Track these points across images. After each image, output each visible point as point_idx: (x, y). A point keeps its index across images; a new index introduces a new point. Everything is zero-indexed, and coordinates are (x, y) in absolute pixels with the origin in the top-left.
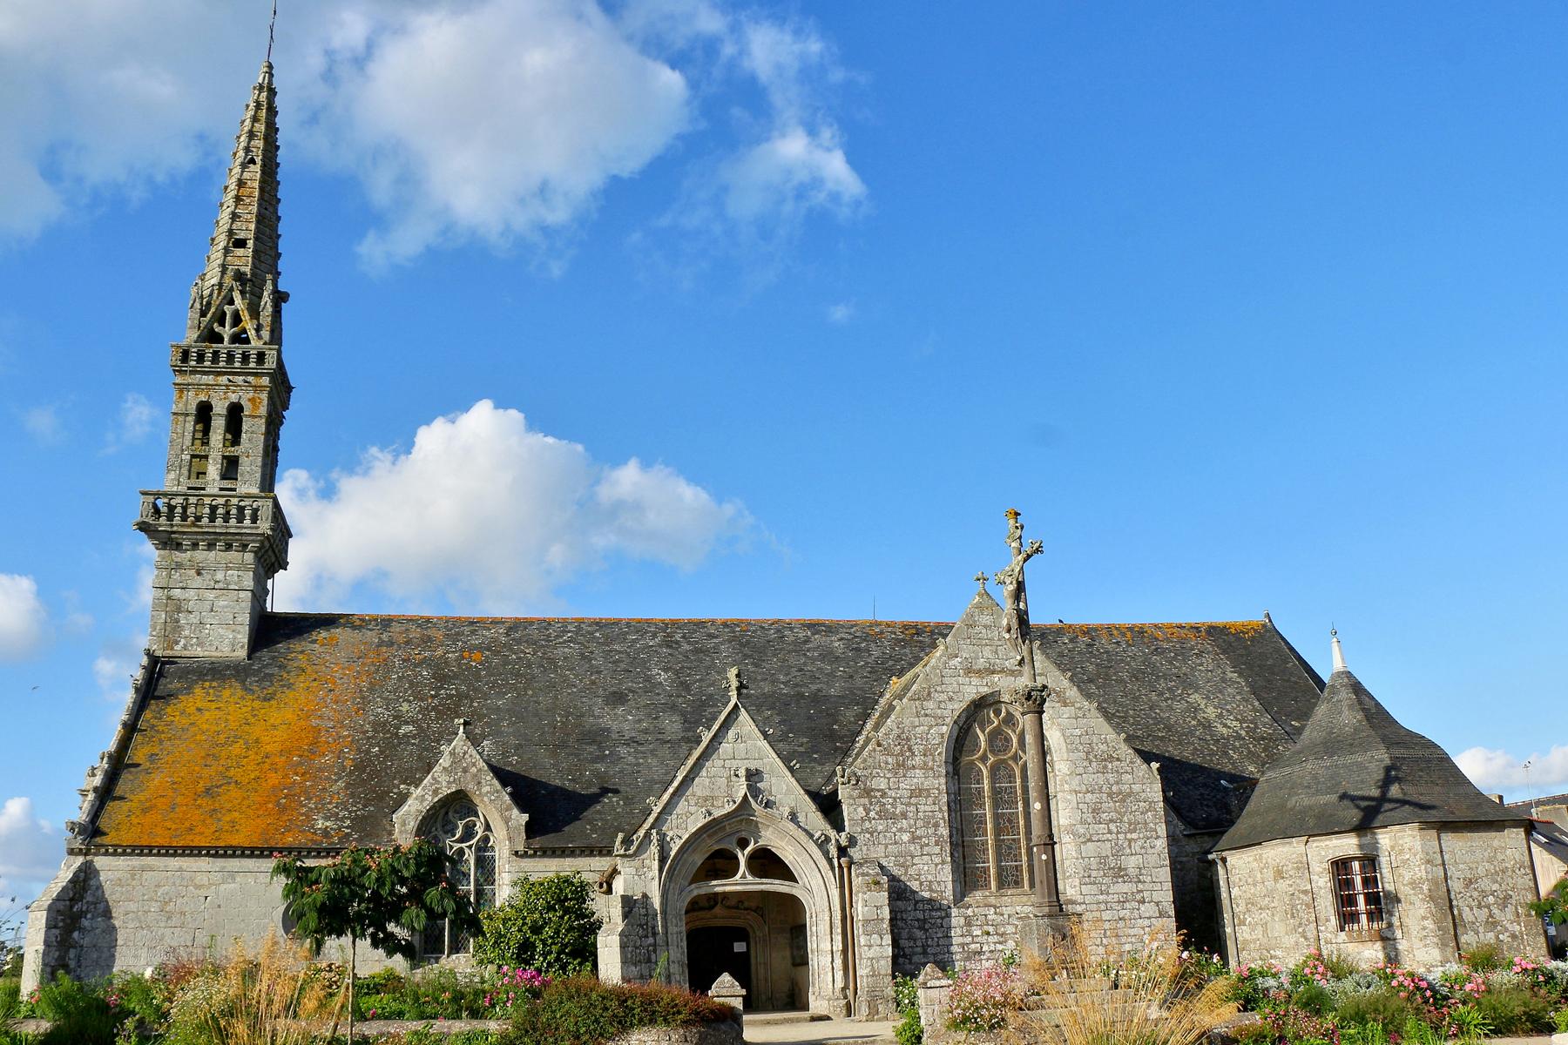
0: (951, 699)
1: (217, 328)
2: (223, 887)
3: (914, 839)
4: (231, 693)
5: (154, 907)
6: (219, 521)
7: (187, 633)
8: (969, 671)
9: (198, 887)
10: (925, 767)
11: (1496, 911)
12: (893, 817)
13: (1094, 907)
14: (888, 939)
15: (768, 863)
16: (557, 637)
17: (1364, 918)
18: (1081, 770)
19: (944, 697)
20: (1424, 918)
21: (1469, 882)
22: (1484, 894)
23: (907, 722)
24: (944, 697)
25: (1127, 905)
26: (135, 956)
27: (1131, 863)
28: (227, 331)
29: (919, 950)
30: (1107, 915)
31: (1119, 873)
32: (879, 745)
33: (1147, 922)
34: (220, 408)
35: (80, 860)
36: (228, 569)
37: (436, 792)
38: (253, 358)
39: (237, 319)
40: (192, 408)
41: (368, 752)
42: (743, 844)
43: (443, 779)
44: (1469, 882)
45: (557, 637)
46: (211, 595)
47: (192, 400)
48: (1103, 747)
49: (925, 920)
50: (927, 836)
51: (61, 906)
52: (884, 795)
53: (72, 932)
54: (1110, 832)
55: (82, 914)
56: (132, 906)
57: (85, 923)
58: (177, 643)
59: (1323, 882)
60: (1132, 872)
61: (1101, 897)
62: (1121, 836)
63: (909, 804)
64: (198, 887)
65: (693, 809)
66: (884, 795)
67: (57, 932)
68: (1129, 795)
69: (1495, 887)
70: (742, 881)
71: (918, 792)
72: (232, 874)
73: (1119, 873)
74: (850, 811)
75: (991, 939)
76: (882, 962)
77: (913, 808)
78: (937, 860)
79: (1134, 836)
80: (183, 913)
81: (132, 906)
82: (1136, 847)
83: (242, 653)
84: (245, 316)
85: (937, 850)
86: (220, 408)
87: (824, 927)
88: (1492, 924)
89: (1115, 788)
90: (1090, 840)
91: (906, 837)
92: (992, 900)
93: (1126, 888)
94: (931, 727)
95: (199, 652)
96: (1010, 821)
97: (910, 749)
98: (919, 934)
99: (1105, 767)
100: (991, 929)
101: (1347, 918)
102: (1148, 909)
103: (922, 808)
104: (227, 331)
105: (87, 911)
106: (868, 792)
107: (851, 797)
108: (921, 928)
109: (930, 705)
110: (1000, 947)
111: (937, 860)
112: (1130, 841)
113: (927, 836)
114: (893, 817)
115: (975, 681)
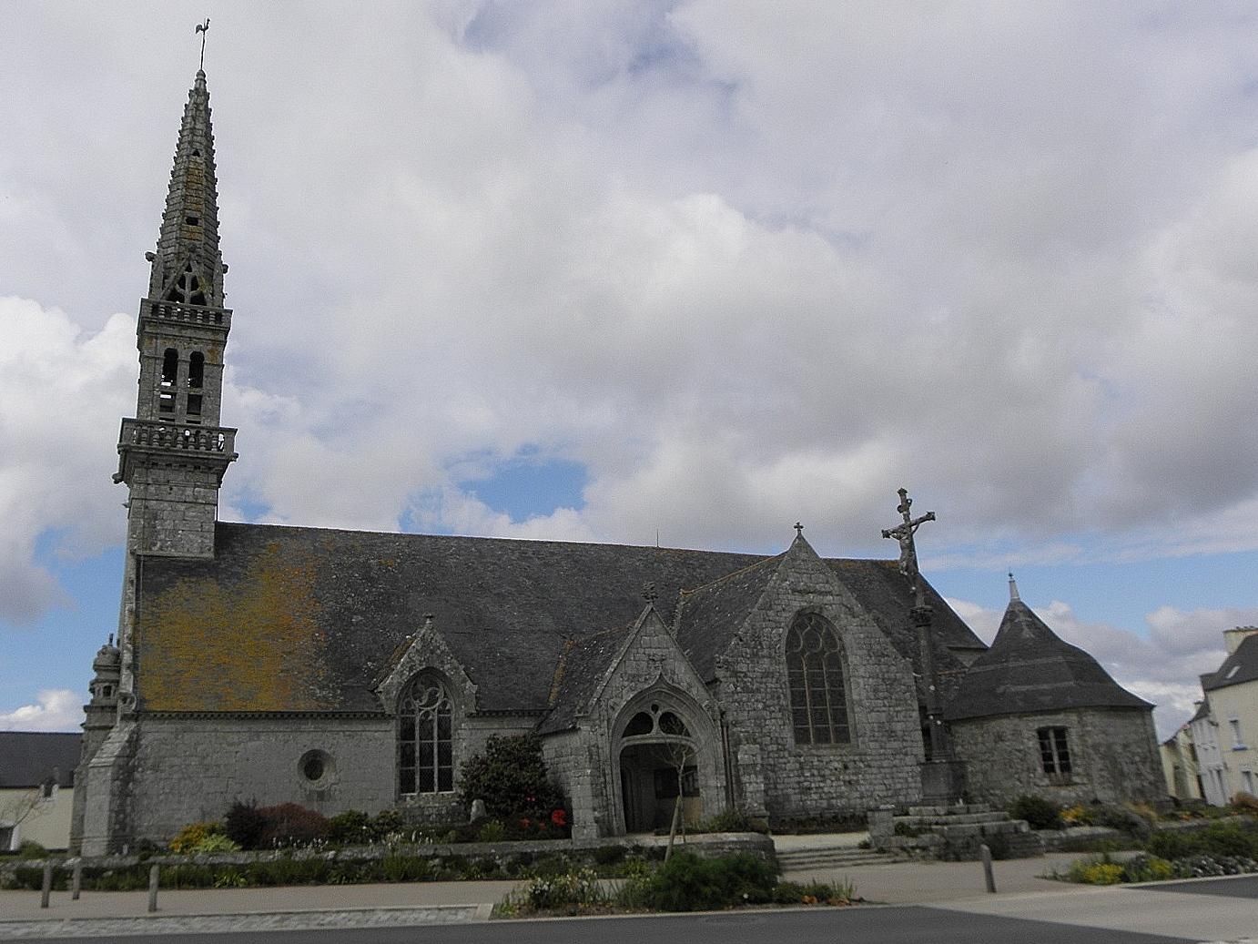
0: (784, 610)
1: (179, 290)
2: (250, 744)
3: (766, 707)
4: (210, 587)
5: (194, 761)
6: (191, 448)
7: (163, 536)
8: (794, 591)
9: (230, 744)
10: (770, 657)
11: (1141, 766)
12: (752, 691)
13: (878, 758)
14: (761, 779)
15: (670, 722)
16: (445, 550)
17: (1058, 771)
18: (865, 662)
19: (780, 608)
20: (1102, 770)
21: (1125, 746)
22: (1134, 754)
23: (758, 624)
24: (780, 608)
25: (898, 757)
26: (179, 802)
27: (898, 727)
28: (188, 292)
29: (772, 786)
30: (885, 764)
31: (891, 734)
32: (741, 640)
33: (909, 769)
34: (184, 355)
35: (133, 725)
36: (196, 486)
37: (411, 669)
38: (212, 318)
39: (195, 285)
40: (161, 354)
41: (334, 636)
42: (655, 708)
43: (416, 658)
44: (1125, 746)
45: (445, 550)
46: (182, 507)
47: (161, 347)
48: (878, 647)
49: (775, 765)
50: (774, 705)
51: (121, 761)
52: (746, 676)
53: (128, 784)
54: (885, 706)
55: (134, 768)
56: (176, 761)
57: (137, 775)
58: (155, 545)
59: (1033, 744)
60: (900, 733)
61: (882, 751)
62: (892, 709)
63: (761, 683)
64: (230, 744)
65: (626, 683)
66: (746, 676)
67: (118, 783)
68: (895, 680)
69: (1139, 750)
70: (655, 736)
71: (766, 674)
72: (258, 733)
73: (891, 734)
74: (728, 686)
75: (816, 779)
76: (758, 795)
77: (763, 686)
78: (781, 722)
79: (899, 708)
80: (218, 766)
81: (176, 761)
82: (901, 717)
83: (210, 555)
84: (202, 281)
85: (780, 715)
86: (184, 355)
87: (710, 770)
88: (1139, 775)
89: (886, 676)
90: (872, 711)
91: (760, 706)
92: (814, 751)
93: (895, 745)
94: (772, 629)
95: (173, 552)
96: (821, 696)
97: (760, 644)
98: (771, 774)
99: (880, 661)
100: (816, 772)
101: (1049, 769)
102: (909, 760)
103: (769, 685)
104: (188, 292)
105: (139, 766)
106: (735, 674)
107: (725, 677)
108: (773, 771)
109: (771, 613)
110: (822, 785)
111: (781, 722)
112: (898, 712)
113: (774, 705)
114: (752, 691)
115: (798, 597)
